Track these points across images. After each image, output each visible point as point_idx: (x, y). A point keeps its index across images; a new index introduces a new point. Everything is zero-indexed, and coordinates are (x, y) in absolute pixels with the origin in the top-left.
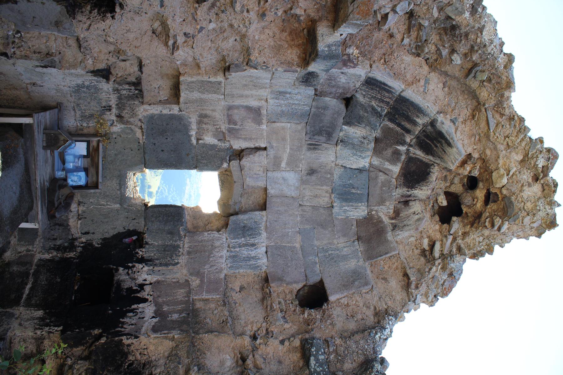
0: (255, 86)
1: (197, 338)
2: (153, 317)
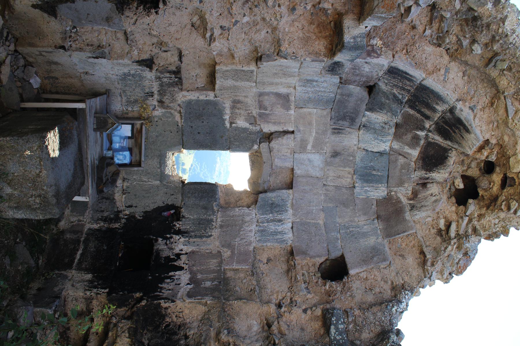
2: (188, 284)
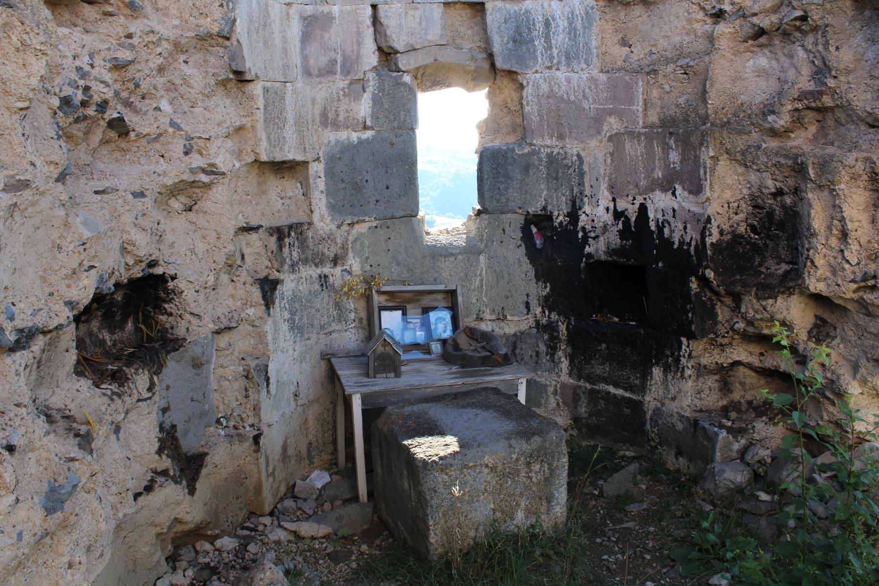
0: (265, 26)
1: (715, 118)
2: (674, 194)
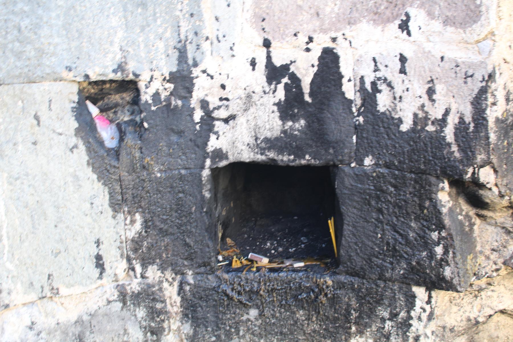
2: (404, 26)
